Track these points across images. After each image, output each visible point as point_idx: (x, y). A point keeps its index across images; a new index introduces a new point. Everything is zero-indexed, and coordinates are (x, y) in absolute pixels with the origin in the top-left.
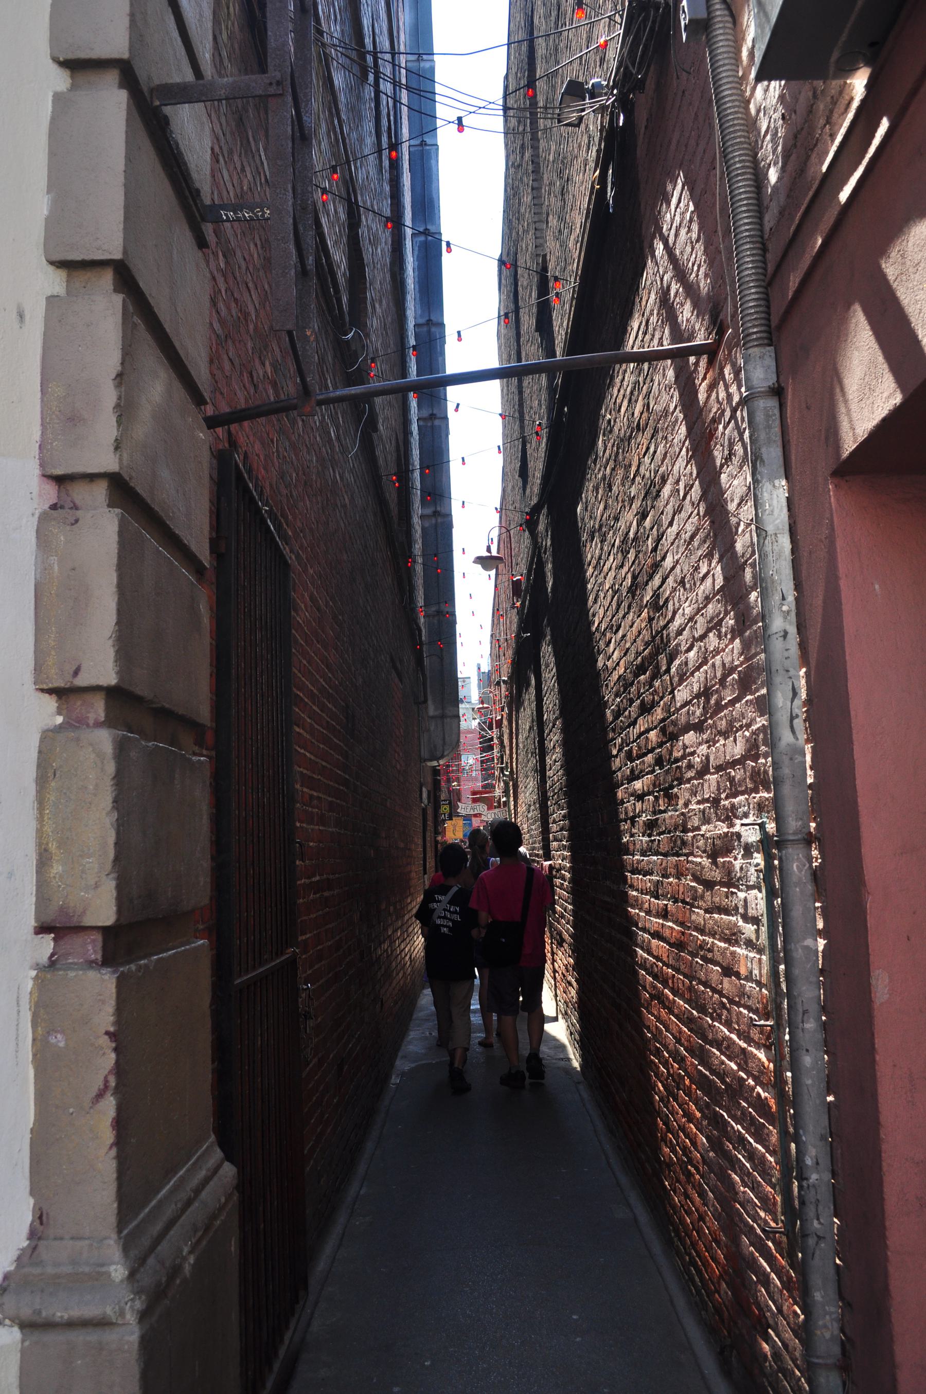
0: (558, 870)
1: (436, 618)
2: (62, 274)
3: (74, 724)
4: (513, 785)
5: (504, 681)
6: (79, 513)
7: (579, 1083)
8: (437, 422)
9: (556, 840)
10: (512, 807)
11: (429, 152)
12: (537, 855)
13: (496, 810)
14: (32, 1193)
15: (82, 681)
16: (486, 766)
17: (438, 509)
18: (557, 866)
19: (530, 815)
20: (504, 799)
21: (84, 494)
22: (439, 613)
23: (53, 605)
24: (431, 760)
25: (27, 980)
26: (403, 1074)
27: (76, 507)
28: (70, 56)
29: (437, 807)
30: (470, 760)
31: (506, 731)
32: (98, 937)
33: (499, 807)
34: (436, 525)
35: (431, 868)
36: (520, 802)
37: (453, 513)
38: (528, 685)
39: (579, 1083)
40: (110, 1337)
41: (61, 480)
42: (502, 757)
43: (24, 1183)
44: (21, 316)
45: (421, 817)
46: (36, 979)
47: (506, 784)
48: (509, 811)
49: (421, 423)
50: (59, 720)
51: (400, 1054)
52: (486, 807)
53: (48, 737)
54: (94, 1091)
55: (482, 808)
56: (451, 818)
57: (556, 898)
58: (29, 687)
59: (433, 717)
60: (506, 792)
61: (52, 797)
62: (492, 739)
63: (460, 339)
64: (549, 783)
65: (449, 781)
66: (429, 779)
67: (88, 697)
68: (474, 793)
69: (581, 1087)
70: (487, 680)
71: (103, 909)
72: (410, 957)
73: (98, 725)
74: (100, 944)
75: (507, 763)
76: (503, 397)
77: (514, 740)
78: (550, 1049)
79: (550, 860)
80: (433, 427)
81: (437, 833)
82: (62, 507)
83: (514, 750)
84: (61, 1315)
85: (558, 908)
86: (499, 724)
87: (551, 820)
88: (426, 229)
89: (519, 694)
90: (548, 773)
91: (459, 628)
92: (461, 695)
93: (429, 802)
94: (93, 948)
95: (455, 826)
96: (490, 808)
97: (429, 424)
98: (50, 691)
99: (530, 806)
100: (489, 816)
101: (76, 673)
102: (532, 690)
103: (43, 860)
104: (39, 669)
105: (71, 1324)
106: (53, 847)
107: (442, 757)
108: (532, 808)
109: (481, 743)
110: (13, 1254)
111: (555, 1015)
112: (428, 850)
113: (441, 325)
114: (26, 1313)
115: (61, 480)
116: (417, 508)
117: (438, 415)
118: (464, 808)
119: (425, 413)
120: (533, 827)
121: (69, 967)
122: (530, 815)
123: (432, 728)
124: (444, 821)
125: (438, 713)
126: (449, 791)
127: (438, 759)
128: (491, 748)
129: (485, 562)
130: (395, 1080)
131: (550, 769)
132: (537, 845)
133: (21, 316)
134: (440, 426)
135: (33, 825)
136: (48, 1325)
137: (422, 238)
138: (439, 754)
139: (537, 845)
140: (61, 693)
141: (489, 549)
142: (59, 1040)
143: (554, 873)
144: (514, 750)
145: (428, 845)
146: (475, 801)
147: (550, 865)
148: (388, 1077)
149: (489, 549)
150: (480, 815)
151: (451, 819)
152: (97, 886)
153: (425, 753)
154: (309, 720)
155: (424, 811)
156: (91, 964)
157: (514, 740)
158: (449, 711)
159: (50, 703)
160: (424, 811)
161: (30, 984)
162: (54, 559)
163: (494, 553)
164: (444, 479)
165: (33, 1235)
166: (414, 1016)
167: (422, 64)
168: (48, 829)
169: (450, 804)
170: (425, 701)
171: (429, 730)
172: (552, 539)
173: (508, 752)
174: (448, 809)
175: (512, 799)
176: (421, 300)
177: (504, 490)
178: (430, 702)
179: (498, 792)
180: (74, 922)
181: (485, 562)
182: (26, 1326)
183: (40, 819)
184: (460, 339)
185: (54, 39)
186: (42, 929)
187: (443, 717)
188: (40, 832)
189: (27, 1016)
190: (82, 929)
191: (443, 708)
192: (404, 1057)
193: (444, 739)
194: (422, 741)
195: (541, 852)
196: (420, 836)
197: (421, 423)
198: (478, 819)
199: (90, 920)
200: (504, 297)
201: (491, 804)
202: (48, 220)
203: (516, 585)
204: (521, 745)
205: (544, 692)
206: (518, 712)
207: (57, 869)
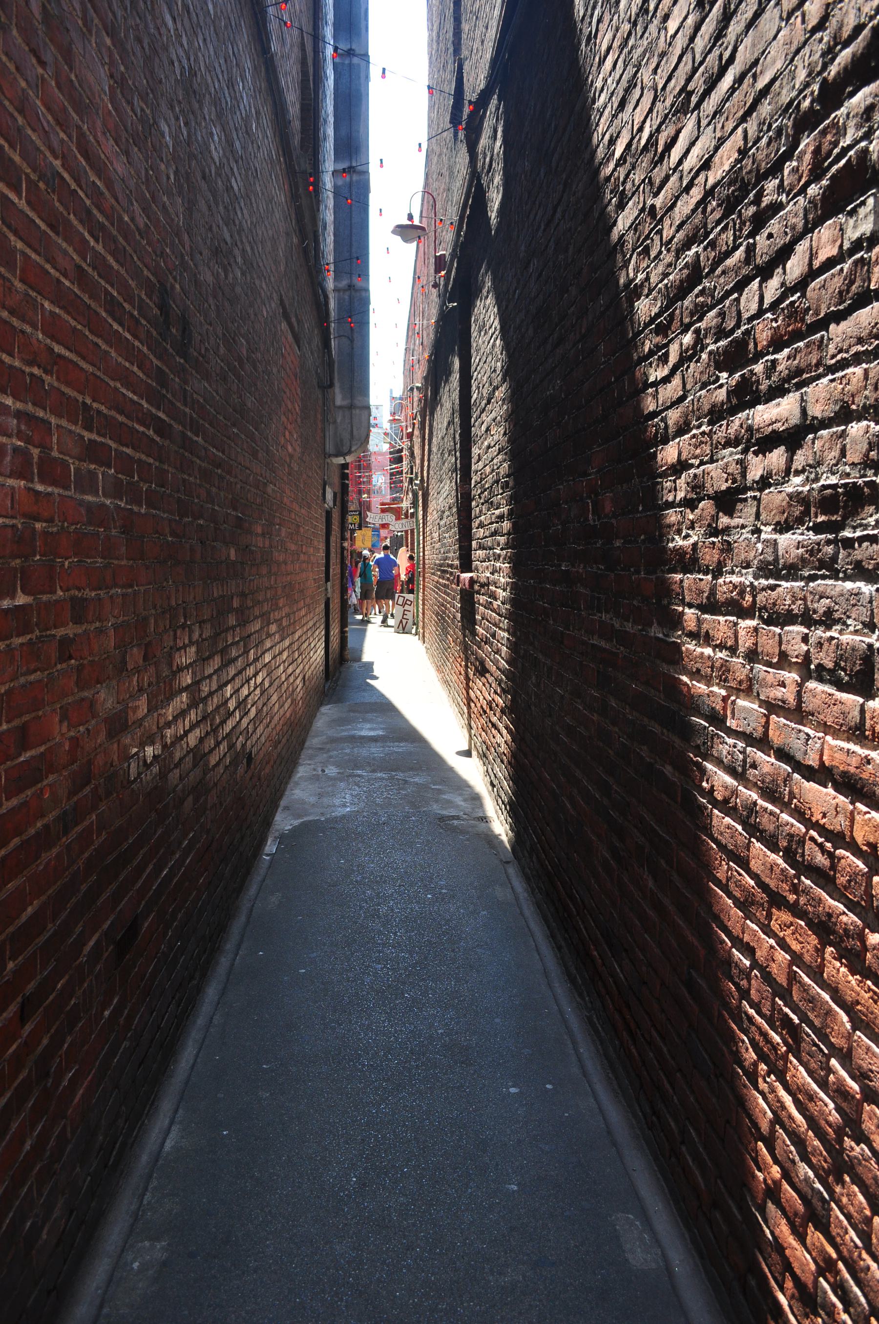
0: (482, 585)
1: (348, 293)
4: (423, 494)
5: (417, 388)
7: (508, 862)
8: (355, 60)
9: (481, 547)
10: (421, 517)
12: (451, 566)
13: (404, 521)
16: (395, 478)
17: (354, 164)
18: (483, 580)
19: (442, 523)
20: (412, 510)
22: (351, 287)
24: (337, 456)
26: (282, 838)
29: (344, 511)
30: (380, 480)
31: (417, 440)
33: (407, 517)
34: (350, 185)
35: (335, 575)
36: (430, 510)
37: (370, 171)
38: (448, 373)
39: (508, 862)
42: (412, 468)
45: (324, 520)
47: (415, 495)
48: (417, 521)
49: (337, 60)
51: (283, 803)
55: (390, 518)
56: (360, 528)
57: (478, 617)
59: (340, 407)
60: (415, 504)
62: (401, 450)
63: (383, 76)
64: (475, 478)
65: (360, 493)
66: (336, 480)
68: (383, 504)
69: (511, 871)
70: (398, 407)
72: (304, 678)
75: (417, 473)
76: (430, 63)
77: (427, 447)
78: (465, 800)
79: (471, 571)
81: (343, 538)
83: (426, 458)
85: (480, 630)
86: (410, 436)
87: (475, 524)
89: (436, 392)
90: (474, 468)
91: (373, 318)
92: (372, 421)
93: (335, 504)
95: (364, 535)
96: (398, 518)
97: (347, 62)
99: (443, 512)
100: (397, 526)
102: (455, 377)
107: (349, 452)
108: (447, 513)
109: (391, 453)
111: (467, 748)
112: (333, 555)
113: (365, 57)
116: (329, 164)
117: (357, 52)
118: (374, 518)
120: (447, 535)
122: (442, 523)
123: (339, 420)
124: (353, 531)
125: (346, 403)
126: (360, 503)
127: (344, 455)
128: (400, 460)
129: (406, 231)
130: (271, 847)
131: (479, 460)
132: (451, 555)
134: (359, 65)
138: (345, 449)
139: (451, 555)
141: (410, 217)
143: (476, 587)
144: (426, 458)
145: (333, 550)
146: (383, 511)
147: (471, 578)
148: (262, 841)
149: (410, 217)
150: (388, 525)
151: (360, 528)
153: (330, 448)
154: (156, 362)
155: (328, 514)
157: (427, 447)
158: (358, 402)
160: (328, 514)
163: (416, 222)
164: (361, 130)
166: (307, 744)
169: (360, 514)
170: (331, 385)
171: (335, 422)
172: (505, 142)
173: (418, 461)
174: (358, 519)
175: (420, 508)
177: (427, 176)
178: (337, 384)
179: (405, 504)
181: (406, 231)
184: (383, 76)
187: (351, 407)
192: (287, 808)
193: (352, 431)
194: (327, 434)
195: (457, 562)
196: (322, 539)
197: (337, 60)
198: (386, 531)
201: (398, 514)
203: (440, 264)
204: (434, 449)
205: (473, 369)
206: (432, 414)
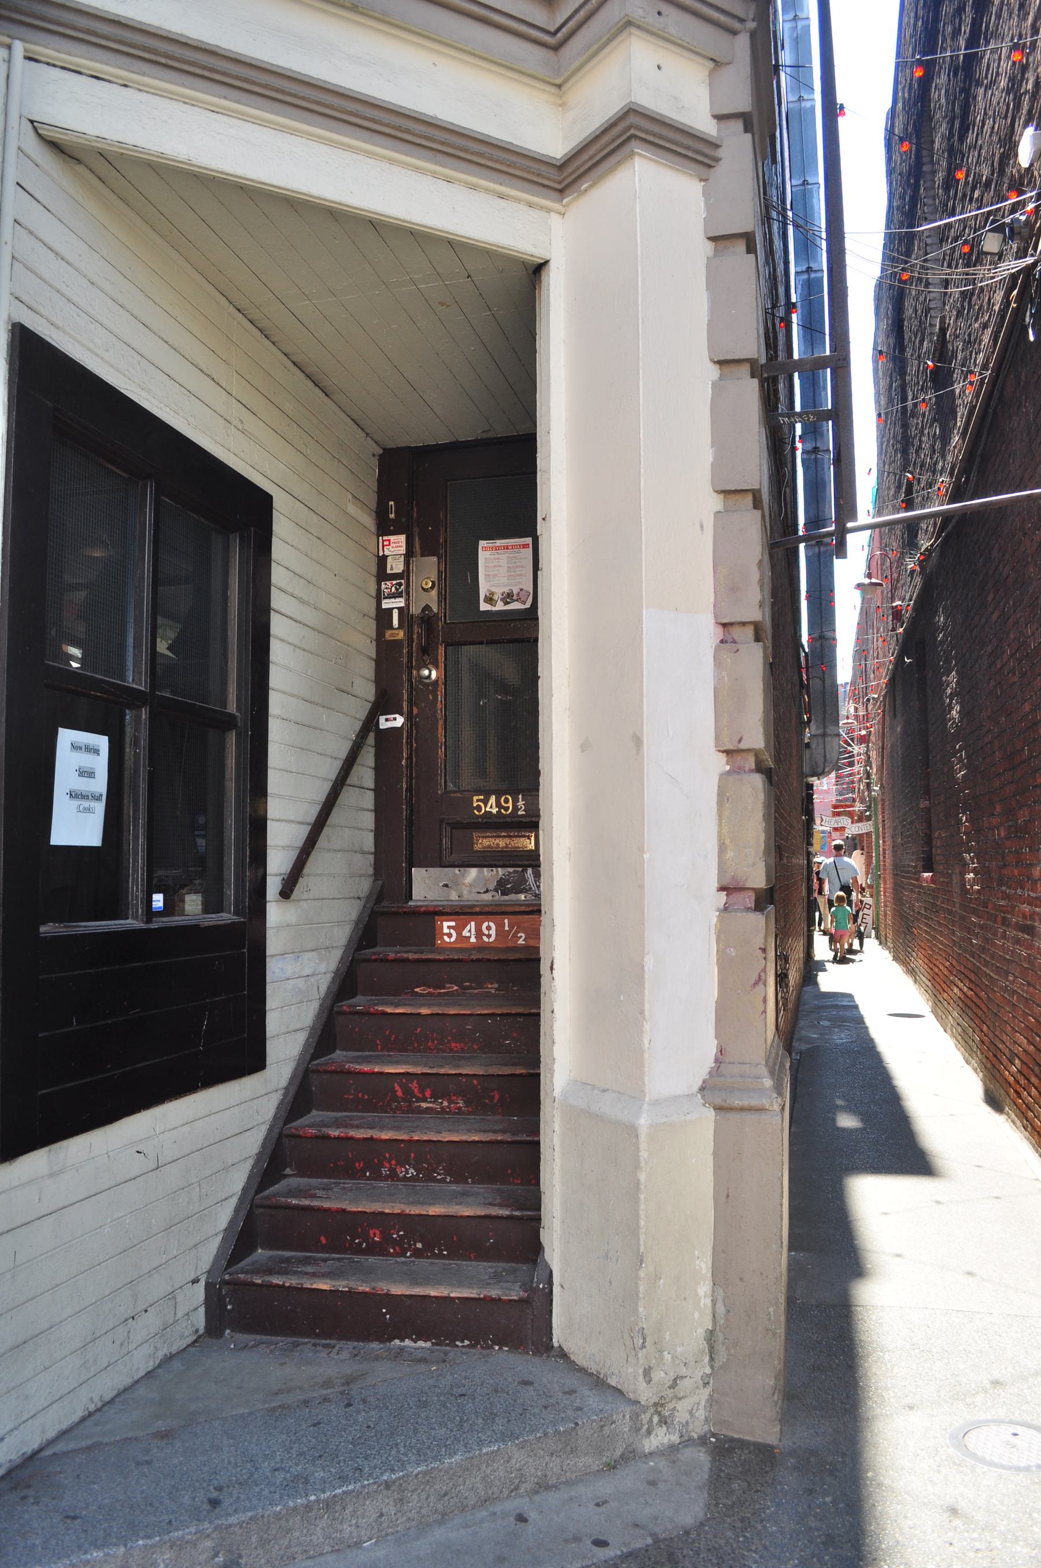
1: (819, 642)
2: (721, 496)
3: (736, 771)
6: (739, 646)
11: (811, 191)
14: (717, 1036)
15: (743, 746)
21: (737, 633)
23: (725, 701)
25: (713, 917)
27: (734, 642)
28: (722, 358)
32: (753, 895)
40: (765, 1117)
41: (725, 625)
43: (712, 1031)
44: (702, 527)
46: (718, 917)
50: (728, 768)
52: (850, 821)
53: (724, 776)
54: (753, 982)
55: (845, 821)
58: (713, 749)
61: (726, 813)
67: (745, 754)
71: (758, 879)
73: (751, 771)
74: (753, 898)
80: (816, 459)
82: (726, 642)
84: (738, 1103)
88: (809, 268)
94: (749, 900)
98: (723, 752)
101: (740, 741)
103: (722, 849)
104: (717, 738)
105: (742, 1109)
106: (728, 841)
110: (707, 1070)
114: (718, 1101)
115: (725, 625)
119: (809, 446)
121: (736, 910)
133: (702, 527)
135: (716, 829)
136: (730, 1109)
137: (805, 276)
138: (820, 770)
140: (728, 752)
142: (732, 952)
152: (754, 864)
153: (806, 769)
156: (748, 909)
159: (723, 757)
161: (715, 920)
162: (724, 674)
165: (716, 1060)
167: (803, 104)
168: (724, 831)
176: (804, 337)
180: (740, 885)
182: (718, 1109)
183: (720, 825)
185: (711, 348)
186: (721, 889)
187: (824, 735)
188: (720, 833)
189: (714, 938)
190: (743, 889)
191: (825, 727)
199: (750, 884)
200: (884, 325)
202: (712, 464)
207: (730, 854)
